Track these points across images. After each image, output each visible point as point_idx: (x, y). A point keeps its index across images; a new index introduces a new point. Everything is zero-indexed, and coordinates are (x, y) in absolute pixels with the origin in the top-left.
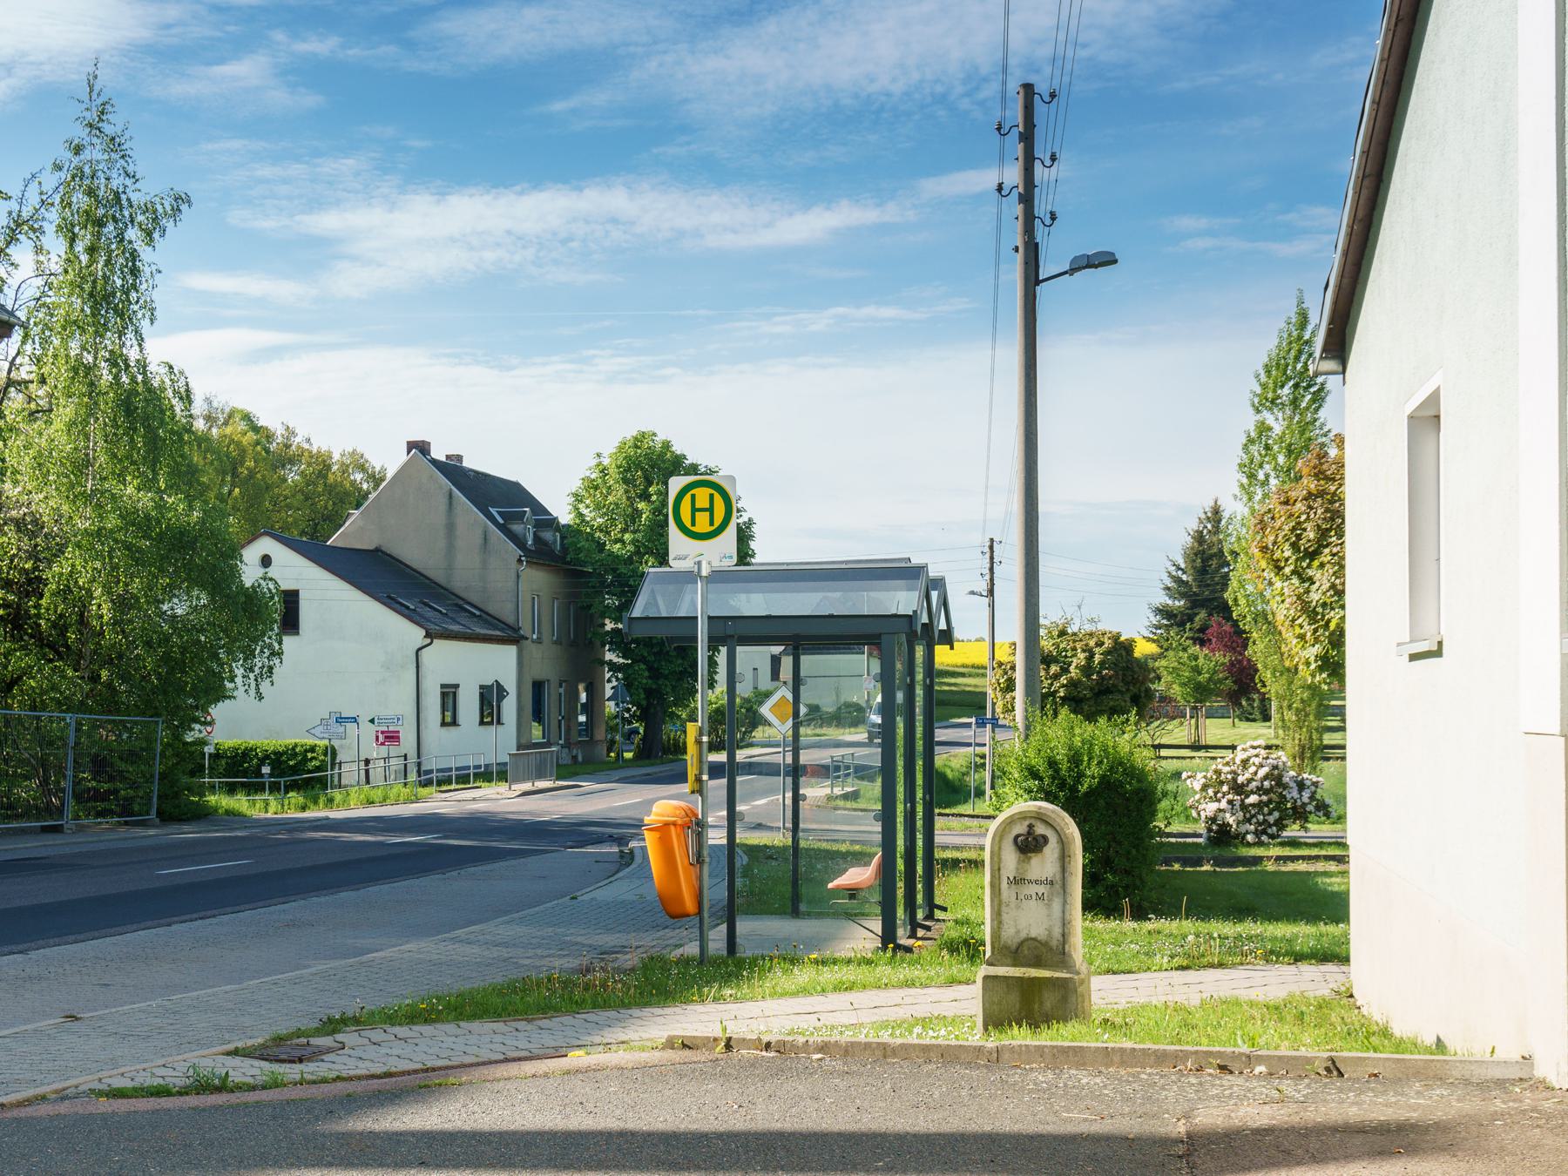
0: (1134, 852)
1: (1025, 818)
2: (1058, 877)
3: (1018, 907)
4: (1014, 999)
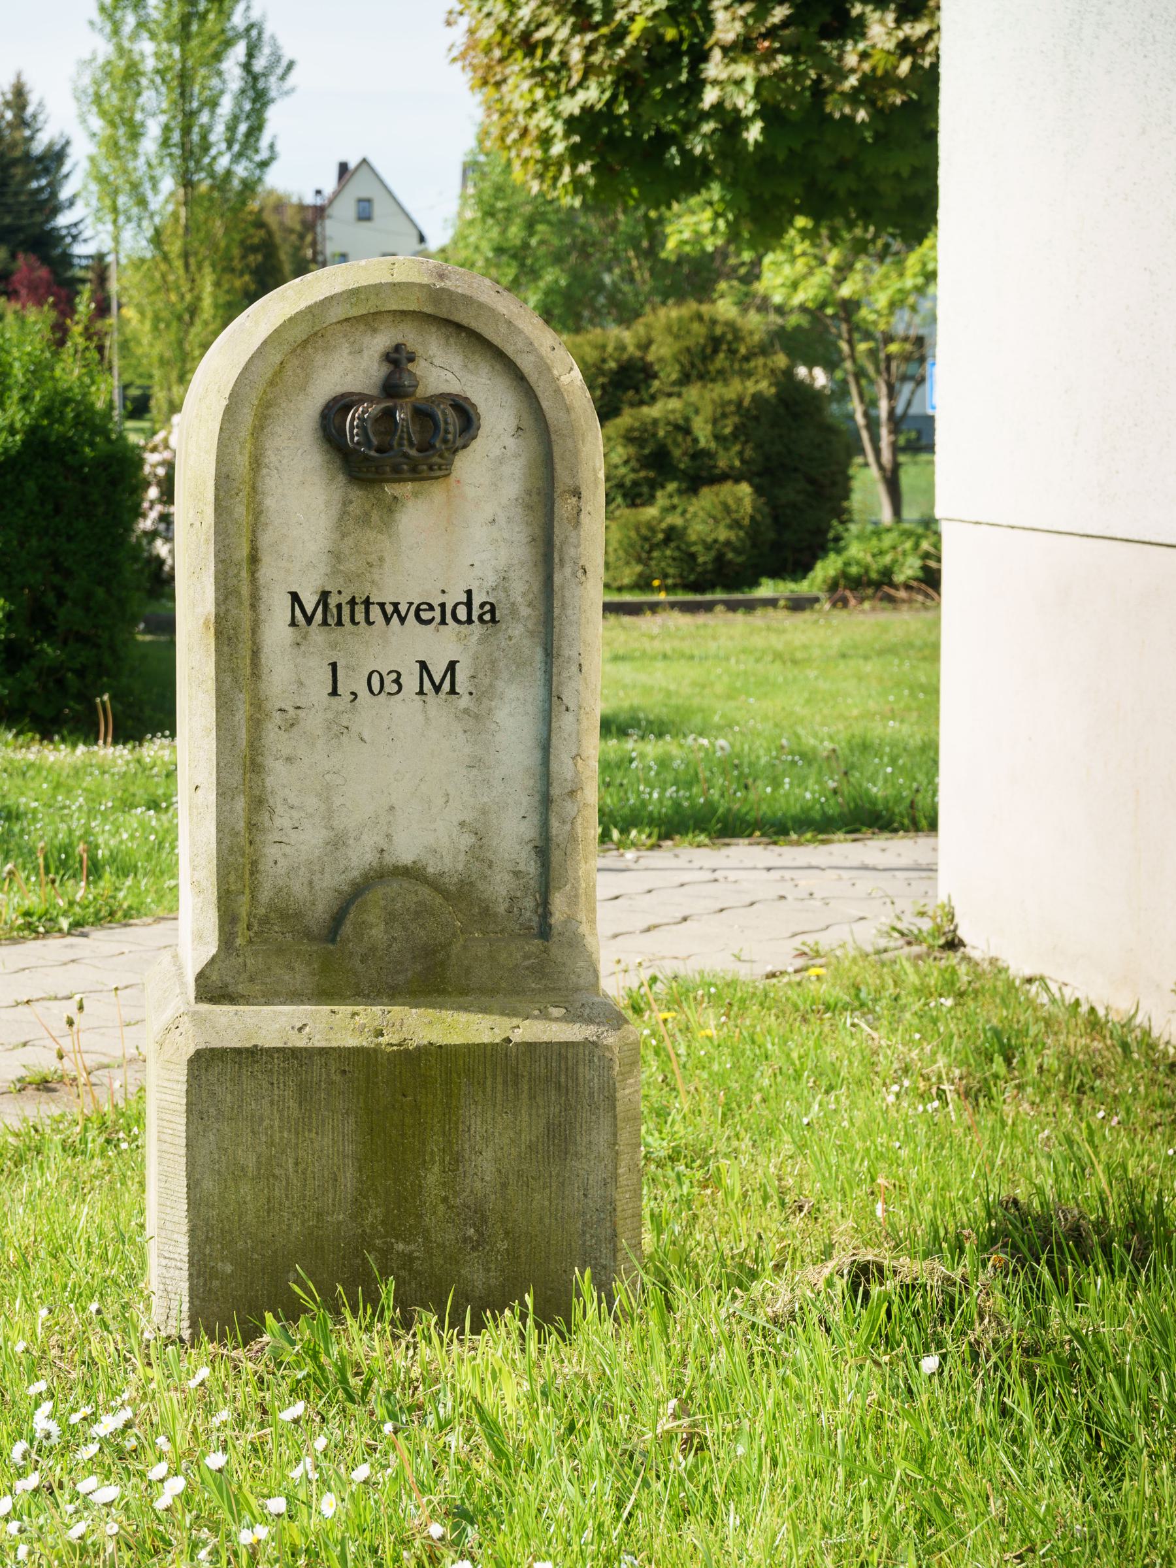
0: (100, 592)
1: (370, 321)
2: (521, 589)
3: (339, 730)
4: (327, 1155)
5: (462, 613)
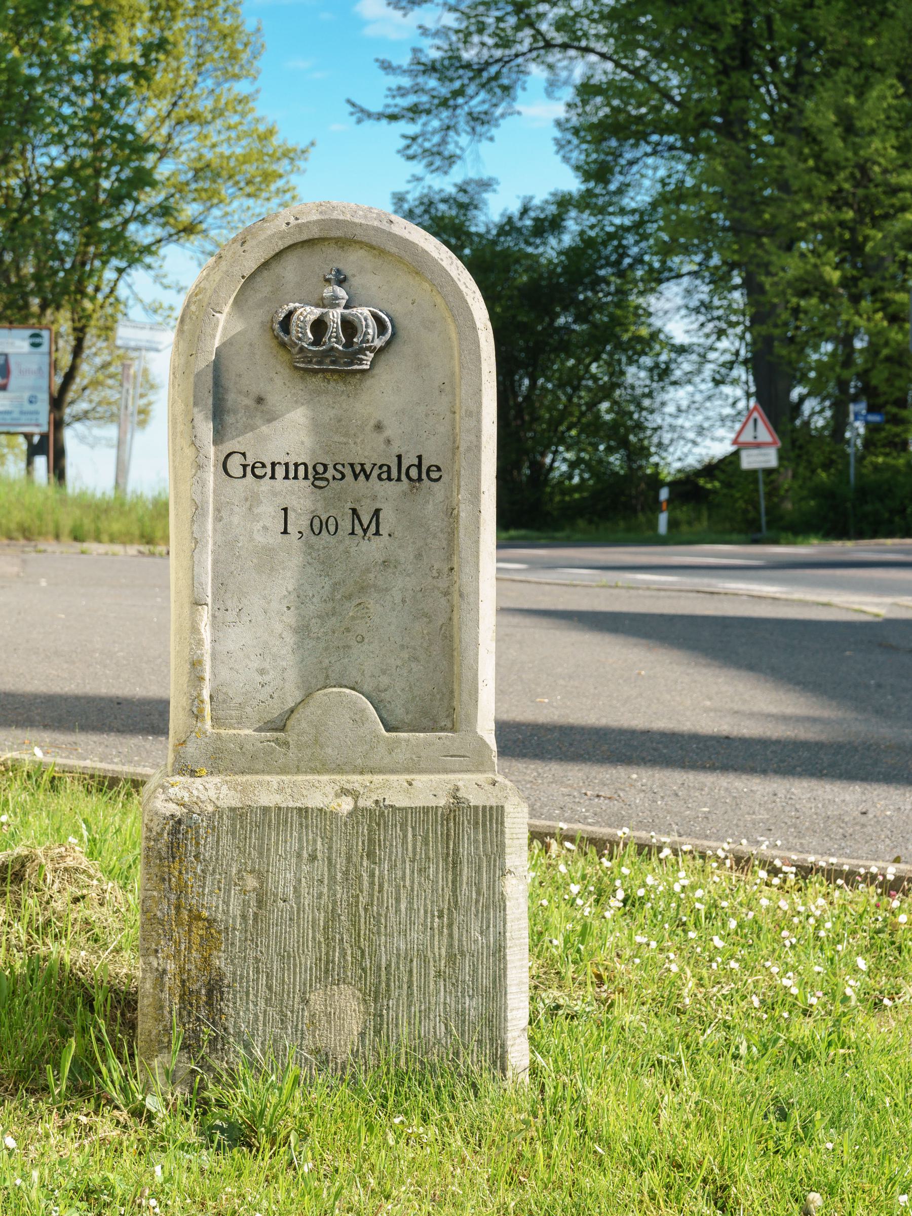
5: (414, 473)
